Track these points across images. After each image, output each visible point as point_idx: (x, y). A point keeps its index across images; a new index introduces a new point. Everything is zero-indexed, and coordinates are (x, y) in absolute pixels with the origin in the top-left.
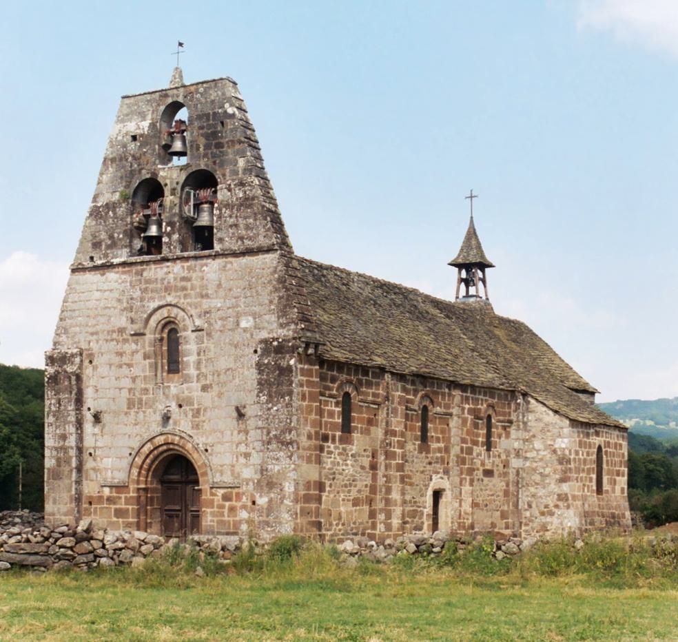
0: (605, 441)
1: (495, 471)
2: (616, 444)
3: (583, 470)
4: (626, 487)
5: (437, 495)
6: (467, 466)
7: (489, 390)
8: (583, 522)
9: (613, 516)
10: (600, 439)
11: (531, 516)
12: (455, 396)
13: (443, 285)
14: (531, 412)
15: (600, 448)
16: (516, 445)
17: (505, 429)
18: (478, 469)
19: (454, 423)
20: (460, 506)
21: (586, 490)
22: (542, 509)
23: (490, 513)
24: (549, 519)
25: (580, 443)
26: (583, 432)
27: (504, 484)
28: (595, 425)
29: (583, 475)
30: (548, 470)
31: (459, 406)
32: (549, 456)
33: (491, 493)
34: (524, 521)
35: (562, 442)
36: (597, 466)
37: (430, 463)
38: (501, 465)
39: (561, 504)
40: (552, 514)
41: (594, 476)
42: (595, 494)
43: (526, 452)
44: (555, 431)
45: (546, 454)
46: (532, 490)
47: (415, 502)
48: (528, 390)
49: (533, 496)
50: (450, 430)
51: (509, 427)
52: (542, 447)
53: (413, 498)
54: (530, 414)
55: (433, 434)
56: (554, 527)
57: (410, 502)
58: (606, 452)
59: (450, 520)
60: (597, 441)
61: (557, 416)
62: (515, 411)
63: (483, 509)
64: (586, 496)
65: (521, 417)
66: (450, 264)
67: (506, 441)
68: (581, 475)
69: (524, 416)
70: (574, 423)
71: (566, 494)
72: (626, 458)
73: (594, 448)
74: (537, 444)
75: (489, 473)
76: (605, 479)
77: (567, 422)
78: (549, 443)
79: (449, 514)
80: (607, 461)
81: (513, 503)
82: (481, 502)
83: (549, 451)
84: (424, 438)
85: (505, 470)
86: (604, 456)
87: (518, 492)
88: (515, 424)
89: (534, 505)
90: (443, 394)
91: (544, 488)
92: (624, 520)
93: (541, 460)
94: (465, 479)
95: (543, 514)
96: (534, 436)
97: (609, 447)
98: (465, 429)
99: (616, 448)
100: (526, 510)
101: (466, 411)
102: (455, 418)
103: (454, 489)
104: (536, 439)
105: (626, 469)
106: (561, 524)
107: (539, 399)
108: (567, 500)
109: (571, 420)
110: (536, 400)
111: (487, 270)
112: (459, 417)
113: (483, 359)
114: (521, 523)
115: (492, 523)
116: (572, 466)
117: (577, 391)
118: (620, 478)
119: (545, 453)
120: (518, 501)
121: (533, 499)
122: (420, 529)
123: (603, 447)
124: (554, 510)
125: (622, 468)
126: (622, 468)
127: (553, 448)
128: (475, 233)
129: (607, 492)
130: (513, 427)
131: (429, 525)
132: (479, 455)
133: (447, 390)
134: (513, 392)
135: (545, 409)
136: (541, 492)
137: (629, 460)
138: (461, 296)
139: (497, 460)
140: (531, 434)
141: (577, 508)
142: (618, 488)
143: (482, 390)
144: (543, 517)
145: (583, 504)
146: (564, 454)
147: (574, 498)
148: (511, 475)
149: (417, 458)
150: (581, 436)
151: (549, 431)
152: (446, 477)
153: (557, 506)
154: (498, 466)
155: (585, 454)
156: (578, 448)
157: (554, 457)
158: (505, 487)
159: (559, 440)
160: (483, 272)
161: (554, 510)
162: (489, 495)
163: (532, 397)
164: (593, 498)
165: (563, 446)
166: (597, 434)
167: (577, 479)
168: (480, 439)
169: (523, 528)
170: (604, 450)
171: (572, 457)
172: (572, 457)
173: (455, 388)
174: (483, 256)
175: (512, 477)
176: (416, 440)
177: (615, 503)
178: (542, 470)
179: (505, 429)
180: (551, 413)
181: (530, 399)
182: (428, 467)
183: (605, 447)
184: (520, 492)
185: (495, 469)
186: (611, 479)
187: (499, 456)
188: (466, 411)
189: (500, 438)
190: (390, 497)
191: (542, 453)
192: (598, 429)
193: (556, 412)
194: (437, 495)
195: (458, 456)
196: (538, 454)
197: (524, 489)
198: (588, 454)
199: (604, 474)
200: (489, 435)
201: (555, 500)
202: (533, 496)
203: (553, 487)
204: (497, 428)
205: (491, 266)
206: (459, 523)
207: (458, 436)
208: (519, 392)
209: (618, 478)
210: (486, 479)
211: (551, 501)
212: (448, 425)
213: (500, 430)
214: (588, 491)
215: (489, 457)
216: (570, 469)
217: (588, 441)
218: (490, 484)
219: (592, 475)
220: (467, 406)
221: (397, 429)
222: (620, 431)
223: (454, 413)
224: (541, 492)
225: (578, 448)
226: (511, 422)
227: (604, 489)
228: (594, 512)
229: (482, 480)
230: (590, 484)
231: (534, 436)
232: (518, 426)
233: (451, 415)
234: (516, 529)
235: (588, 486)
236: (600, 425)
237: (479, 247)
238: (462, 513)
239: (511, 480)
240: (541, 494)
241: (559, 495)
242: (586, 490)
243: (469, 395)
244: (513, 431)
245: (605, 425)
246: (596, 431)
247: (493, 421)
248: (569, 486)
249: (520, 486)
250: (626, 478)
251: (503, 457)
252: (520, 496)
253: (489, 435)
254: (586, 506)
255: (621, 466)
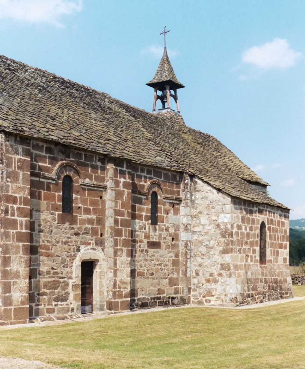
0: (268, 219)
1: (162, 243)
2: (279, 222)
3: (246, 243)
4: (288, 257)
5: (88, 267)
6: (123, 238)
7: (155, 170)
8: (246, 288)
9: (276, 282)
10: (263, 216)
11: (199, 283)
12: (109, 169)
13: (145, 100)
14: (197, 191)
15: (263, 225)
16: (185, 220)
17: (173, 206)
18: (141, 241)
19: (109, 195)
20: (115, 275)
21: (249, 260)
22: (208, 276)
23: (156, 281)
24: (213, 286)
25: (243, 220)
26: (246, 210)
27: (172, 254)
28: (257, 204)
29: (247, 247)
30: (212, 243)
31: (112, 180)
32: (213, 230)
33: (157, 263)
34: (192, 287)
35: (225, 217)
36: (261, 240)
37: (77, 234)
38: (169, 239)
39: (223, 272)
40: (216, 282)
41: (258, 249)
42: (259, 264)
43: (194, 227)
44: (219, 207)
45: (211, 228)
46: (199, 260)
47: (56, 273)
48: (197, 173)
49: (200, 265)
50: (104, 203)
51: (179, 204)
52: (207, 222)
53: (53, 269)
54: (197, 193)
55: (80, 205)
56: (217, 293)
57: (48, 273)
58: (269, 228)
59: (105, 289)
60: (260, 218)
61: (220, 194)
62: (183, 191)
63: (148, 278)
64: (249, 265)
65: (188, 196)
66: (148, 85)
67: (175, 217)
68: (244, 247)
69: (191, 195)
70: (236, 200)
71: (228, 264)
72: (288, 234)
73: (258, 223)
74: (203, 220)
75: (154, 245)
76: (268, 251)
77: (230, 199)
78: (214, 218)
79: (104, 283)
80: (270, 236)
81: (183, 271)
82: (146, 271)
83: (213, 225)
84: (67, 206)
85: (173, 243)
86: (267, 231)
87: (187, 261)
88: (183, 202)
89: (201, 273)
90: (94, 168)
91: (209, 258)
92: (286, 285)
93: (207, 233)
94: (122, 250)
95: (208, 281)
96: (200, 213)
97: (272, 224)
98: (120, 202)
99: (279, 225)
100: (195, 278)
101: (121, 185)
102: (109, 191)
103: (109, 259)
104: (203, 215)
105: (288, 243)
106: (224, 290)
107: (205, 179)
108: (229, 269)
109: (232, 197)
110: (202, 180)
111: (178, 90)
112: (112, 190)
113: (158, 147)
114: (189, 289)
115: (159, 290)
116: (235, 238)
117: (250, 182)
118: (283, 250)
119: (210, 227)
120: (186, 270)
121: (200, 268)
122: (65, 299)
123: (266, 224)
124: (218, 278)
125: (285, 242)
126: (285, 242)
127: (217, 223)
128: (168, 60)
129: (270, 261)
130: (182, 205)
131: (76, 296)
132: (143, 228)
133: (99, 164)
134: (181, 173)
135: (210, 188)
136: (207, 262)
137: (291, 235)
138: (157, 110)
139: (164, 234)
140: (198, 211)
141: (239, 276)
142: (281, 259)
143: (146, 168)
144: (208, 284)
145: (246, 273)
146: (226, 228)
147: (236, 267)
148: (180, 247)
149: (56, 228)
150: (244, 213)
151: (213, 207)
152: (99, 248)
153: (220, 275)
154: (165, 238)
155: (248, 229)
156: (240, 223)
157: (218, 231)
158: (174, 258)
159: (222, 216)
160: (175, 91)
161: (218, 278)
162: (155, 265)
163: (199, 178)
164: (256, 267)
165: (226, 221)
166: (260, 212)
167: (240, 251)
168: (144, 214)
169: (192, 293)
170: (267, 226)
171: (234, 231)
172: (234, 231)
173: (108, 162)
174: (174, 77)
175: (181, 249)
176: (57, 209)
177: (278, 271)
178: (207, 243)
179: (173, 206)
180: (215, 191)
181: (196, 180)
182: (74, 238)
183: (268, 224)
184: (188, 263)
185: (162, 241)
186: (274, 251)
187: (167, 230)
188: (121, 185)
189: (168, 214)
190: (8, 269)
191: (207, 227)
192: (261, 208)
193: (219, 190)
194: (88, 267)
195: (111, 228)
196: (204, 228)
197: (192, 259)
198: (251, 229)
199: (267, 246)
200: (154, 210)
201: (218, 270)
202: (200, 265)
203: (218, 258)
204: (164, 204)
205: (181, 86)
206: (114, 293)
207: (111, 208)
208: (187, 173)
209: (280, 250)
210: (151, 251)
211: (216, 269)
212: (101, 198)
213: (168, 206)
214: (251, 261)
215: (155, 230)
216: (232, 241)
217: (251, 217)
218: (156, 255)
219: (255, 248)
220: (122, 180)
221: (18, 196)
222: (282, 211)
223: (108, 187)
224: (207, 262)
225: (240, 223)
226: (180, 200)
227: (267, 259)
228: (258, 279)
229: (147, 252)
230: (254, 255)
231: (200, 213)
232: (187, 204)
233: (105, 188)
234: (185, 294)
235: (252, 257)
236: (263, 204)
237: (171, 70)
238: (118, 282)
239: (181, 251)
240: (207, 264)
241: (222, 265)
242: (249, 260)
243: (124, 169)
244: (182, 209)
245: (268, 205)
246: (259, 209)
247: (159, 197)
248: (231, 257)
249: (188, 257)
250: (288, 250)
251: (172, 231)
252: (188, 265)
253: (154, 210)
254: (249, 274)
255: (283, 240)
